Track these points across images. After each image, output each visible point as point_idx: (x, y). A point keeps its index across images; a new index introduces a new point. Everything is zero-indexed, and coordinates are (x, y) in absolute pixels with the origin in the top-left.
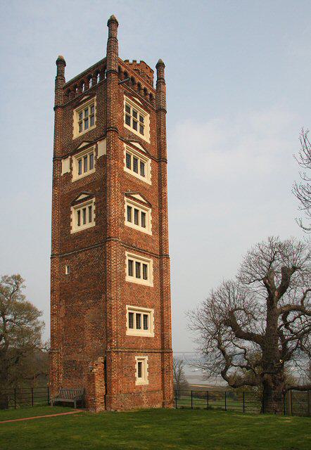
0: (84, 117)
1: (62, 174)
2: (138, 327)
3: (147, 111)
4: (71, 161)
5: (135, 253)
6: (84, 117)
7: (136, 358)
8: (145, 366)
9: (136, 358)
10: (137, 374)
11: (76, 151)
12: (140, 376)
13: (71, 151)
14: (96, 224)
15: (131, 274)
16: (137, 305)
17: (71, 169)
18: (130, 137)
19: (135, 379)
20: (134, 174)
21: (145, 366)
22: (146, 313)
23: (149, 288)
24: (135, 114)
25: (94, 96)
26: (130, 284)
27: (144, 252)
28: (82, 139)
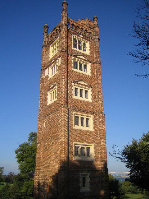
0: (54, 48)
1: (45, 77)
2: (82, 125)
3: (87, 40)
4: (48, 70)
5: (80, 113)
6: (54, 48)
7: (81, 174)
8: (88, 180)
9: (81, 174)
10: (81, 185)
11: (51, 64)
12: (84, 186)
13: (48, 64)
14: (57, 99)
15: (76, 94)
16: (82, 142)
17: (48, 74)
18: (76, 53)
19: (79, 187)
20: (80, 71)
21: (88, 180)
22: (88, 118)
23: (90, 132)
24: (80, 42)
25: (57, 38)
26: (76, 130)
27: (86, 112)
28: (53, 59)
